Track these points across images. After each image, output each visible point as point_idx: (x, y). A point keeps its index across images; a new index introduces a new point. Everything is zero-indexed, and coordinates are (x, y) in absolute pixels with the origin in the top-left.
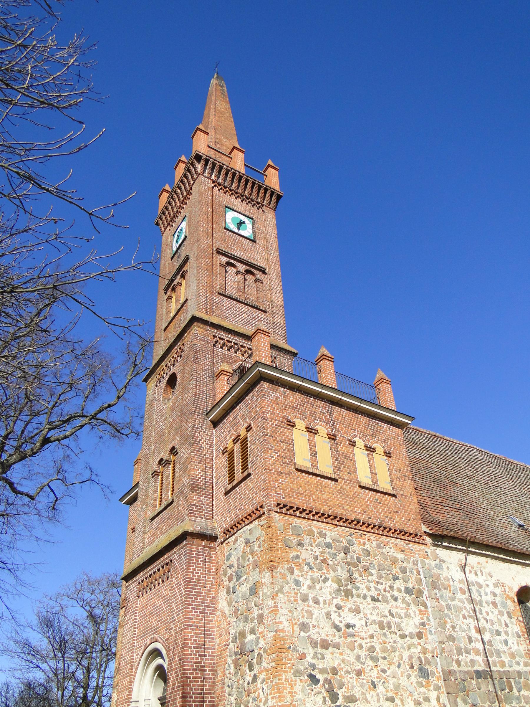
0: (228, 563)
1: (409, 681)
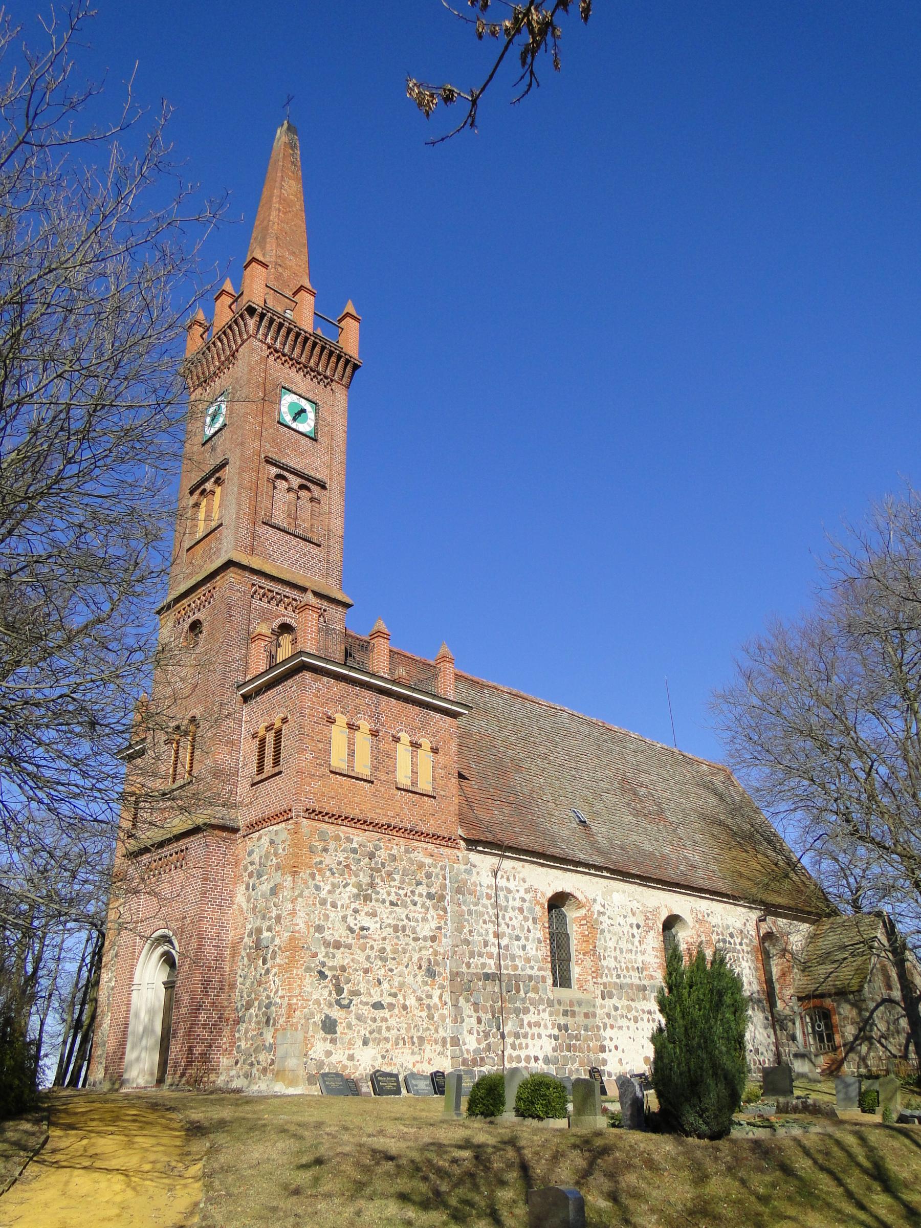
0: (249, 859)
1: (415, 980)
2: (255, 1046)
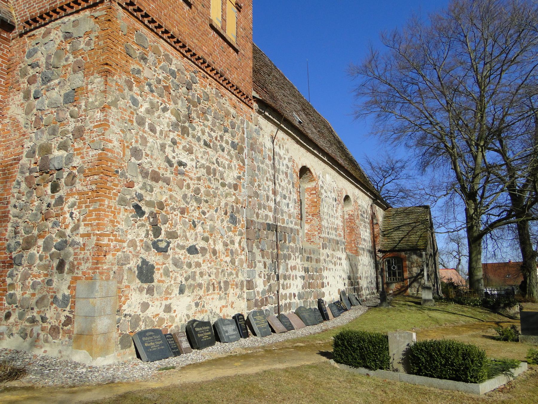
2: (37, 297)
